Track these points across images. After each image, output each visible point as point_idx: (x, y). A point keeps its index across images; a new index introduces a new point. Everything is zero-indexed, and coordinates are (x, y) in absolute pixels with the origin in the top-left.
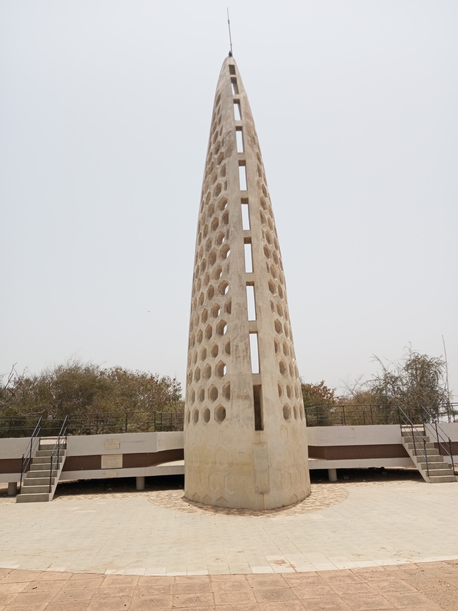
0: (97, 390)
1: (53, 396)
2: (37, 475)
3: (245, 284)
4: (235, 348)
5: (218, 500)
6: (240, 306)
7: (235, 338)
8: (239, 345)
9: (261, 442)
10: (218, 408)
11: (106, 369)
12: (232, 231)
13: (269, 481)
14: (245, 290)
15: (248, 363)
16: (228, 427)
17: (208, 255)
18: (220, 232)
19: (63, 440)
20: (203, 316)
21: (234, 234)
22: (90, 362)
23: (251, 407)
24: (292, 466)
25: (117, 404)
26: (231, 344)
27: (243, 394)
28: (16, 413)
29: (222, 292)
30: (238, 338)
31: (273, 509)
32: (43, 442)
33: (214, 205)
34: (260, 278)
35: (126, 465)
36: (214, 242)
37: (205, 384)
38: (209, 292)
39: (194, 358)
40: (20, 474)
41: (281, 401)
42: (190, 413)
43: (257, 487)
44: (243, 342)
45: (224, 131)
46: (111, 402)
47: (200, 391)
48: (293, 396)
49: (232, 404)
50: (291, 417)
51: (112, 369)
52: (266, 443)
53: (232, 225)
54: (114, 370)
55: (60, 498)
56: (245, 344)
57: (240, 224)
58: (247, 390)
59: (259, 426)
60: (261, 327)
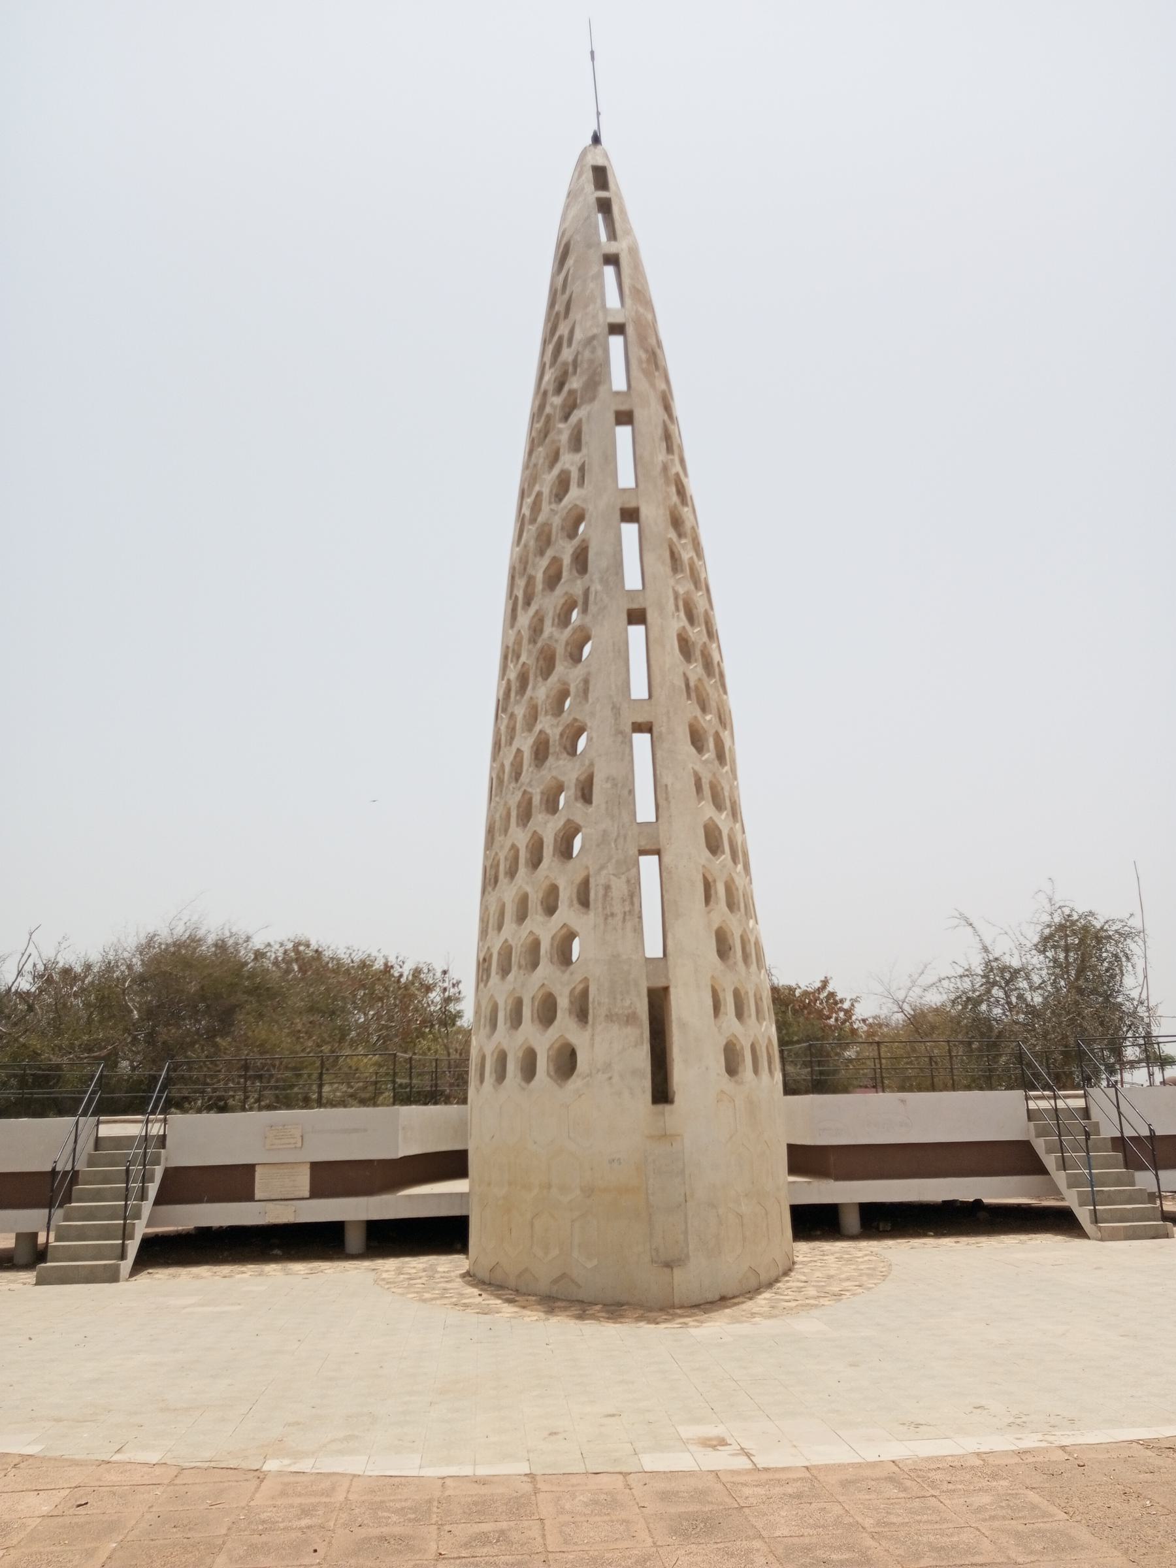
0: (245, 997)
1: (132, 1011)
2: (90, 1214)
3: (628, 728)
4: (601, 892)
5: (555, 1281)
6: (615, 785)
7: (602, 867)
10: (557, 1046)
11: (269, 945)
12: (596, 593)
13: (686, 1232)
15: (635, 930)
18: (566, 593)
19: (157, 1125)
21: (601, 600)
25: (295, 1034)
26: (592, 880)
27: (621, 1012)
29: (570, 750)
30: (611, 868)
31: (697, 1306)
32: (106, 1131)
34: (668, 712)
35: (317, 1191)
38: (537, 749)
40: (47, 1211)
41: (720, 1028)
42: (483, 1058)
43: (657, 1250)
44: (624, 878)
45: (578, 335)
46: (281, 1029)
47: (510, 1001)
48: (750, 1016)
49: (593, 1035)
51: (285, 943)
52: (679, 1135)
53: (596, 577)
54: (290, 946)
55: (149, 1273)
56: (628, 881)
57: (617, 574)
59: (662, 1093)
60: (670, 839)
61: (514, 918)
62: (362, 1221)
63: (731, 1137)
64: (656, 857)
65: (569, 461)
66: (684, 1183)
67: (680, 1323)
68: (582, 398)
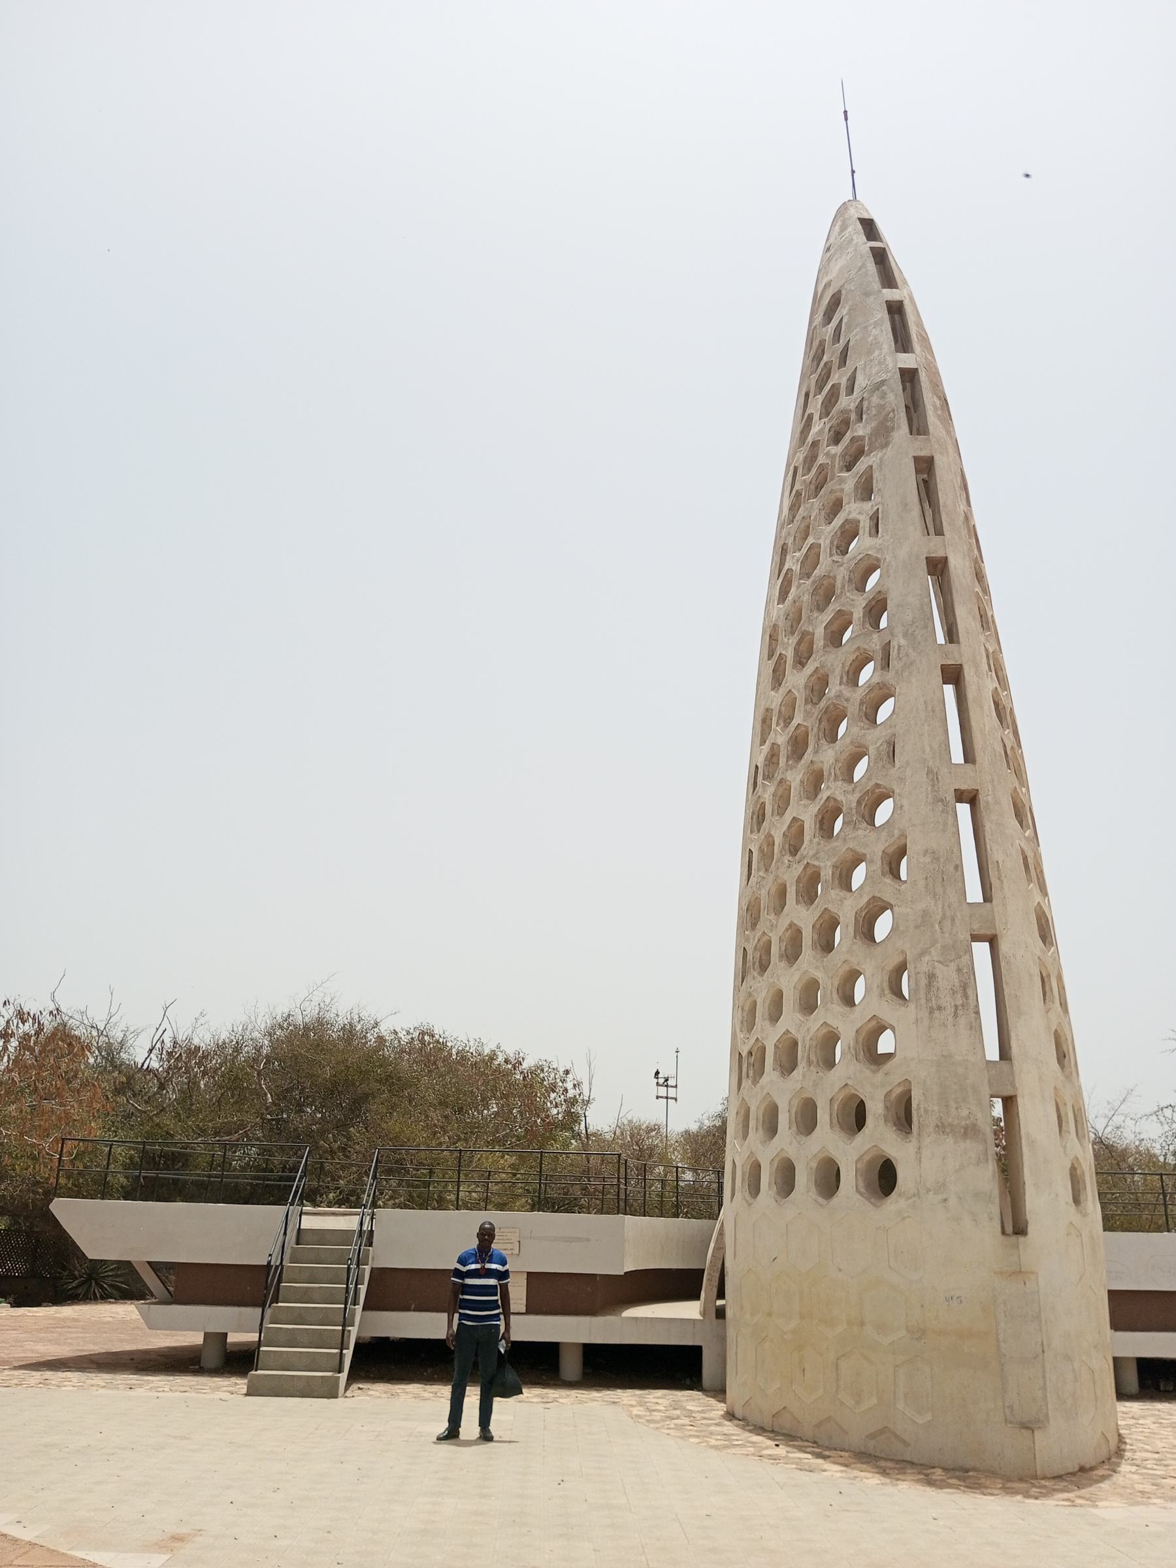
0: (376, 1086)
1: (266, 1095)
2: (300, 1317)
3: (950, 797)
5: (872, 1436)
6: (936, 859)
7: (923, 953)
8: (938, 972)
9: (1021, 1272)
10: (867, 1158)
12: (899, 647)
13: (1044, 1388)
14: (950, 812)
16: (908, 1217)
17: (816, 711)
20: (801, 885)
21: (907, 655)
22: (355, 1011)
23: (987, 1161)
24: (1096, 1347)
27: (956, 1122)
28: (170, 1134)
30: (935, 953)
31: (1059, 1477)
32: (308, 1223)
33: (834, 578)
36: (839, 678)
37: (816, 1084)
38: (823, 818)
39: (767, 1005)
43: (1011, 1407)
44: (953, 966)
45: (861, 381)
47: (796, 1102)
49: (919, 1148)
50: (1087, 1200)
51: (411, 1031)
52: (1033, 1273)
54: (416, 1035)
55: (359, 1388)
56: (959, 970)
57: (926, 627)
58: (969, 1109)
60: (1006, 923)
61: (797, 1008)
62: (579, 1344)
63: (1081, 1279)
64: (987, 945)
65: (855, 510)
66: (1041, 1330)
67: (1063, 1500)
68: (870, 445)
